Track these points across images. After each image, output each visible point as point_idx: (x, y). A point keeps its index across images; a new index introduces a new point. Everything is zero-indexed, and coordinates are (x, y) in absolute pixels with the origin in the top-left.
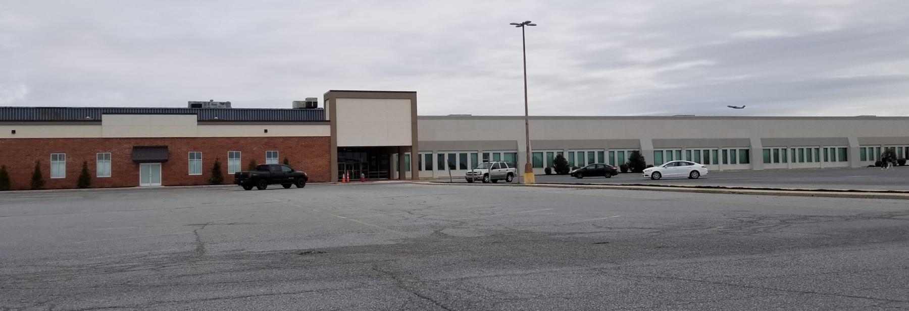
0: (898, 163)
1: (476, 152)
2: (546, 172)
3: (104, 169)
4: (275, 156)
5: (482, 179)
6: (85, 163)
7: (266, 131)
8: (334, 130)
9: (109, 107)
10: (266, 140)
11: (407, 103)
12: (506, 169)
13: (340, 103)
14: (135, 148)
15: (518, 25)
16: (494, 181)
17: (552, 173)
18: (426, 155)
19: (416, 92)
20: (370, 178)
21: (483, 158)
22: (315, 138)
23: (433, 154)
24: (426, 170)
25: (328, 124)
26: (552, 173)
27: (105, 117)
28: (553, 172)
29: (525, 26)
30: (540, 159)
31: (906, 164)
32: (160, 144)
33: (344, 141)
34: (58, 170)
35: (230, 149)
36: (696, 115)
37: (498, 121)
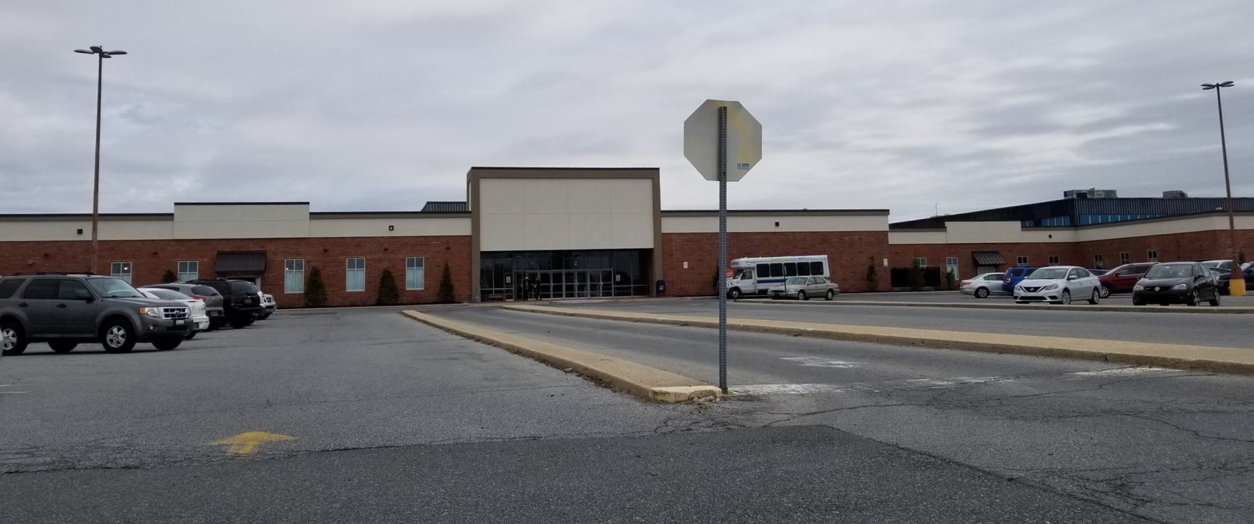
4: (193, 268)
7: (777, 224)
8: (476, 226)
9: (1137, 197)
11: (647, 184)
15: (1209, 87)
19: (658, 169)
20: (567, 297)
22: (48, 245)
25: (1226, 215)
33: (489, 243)
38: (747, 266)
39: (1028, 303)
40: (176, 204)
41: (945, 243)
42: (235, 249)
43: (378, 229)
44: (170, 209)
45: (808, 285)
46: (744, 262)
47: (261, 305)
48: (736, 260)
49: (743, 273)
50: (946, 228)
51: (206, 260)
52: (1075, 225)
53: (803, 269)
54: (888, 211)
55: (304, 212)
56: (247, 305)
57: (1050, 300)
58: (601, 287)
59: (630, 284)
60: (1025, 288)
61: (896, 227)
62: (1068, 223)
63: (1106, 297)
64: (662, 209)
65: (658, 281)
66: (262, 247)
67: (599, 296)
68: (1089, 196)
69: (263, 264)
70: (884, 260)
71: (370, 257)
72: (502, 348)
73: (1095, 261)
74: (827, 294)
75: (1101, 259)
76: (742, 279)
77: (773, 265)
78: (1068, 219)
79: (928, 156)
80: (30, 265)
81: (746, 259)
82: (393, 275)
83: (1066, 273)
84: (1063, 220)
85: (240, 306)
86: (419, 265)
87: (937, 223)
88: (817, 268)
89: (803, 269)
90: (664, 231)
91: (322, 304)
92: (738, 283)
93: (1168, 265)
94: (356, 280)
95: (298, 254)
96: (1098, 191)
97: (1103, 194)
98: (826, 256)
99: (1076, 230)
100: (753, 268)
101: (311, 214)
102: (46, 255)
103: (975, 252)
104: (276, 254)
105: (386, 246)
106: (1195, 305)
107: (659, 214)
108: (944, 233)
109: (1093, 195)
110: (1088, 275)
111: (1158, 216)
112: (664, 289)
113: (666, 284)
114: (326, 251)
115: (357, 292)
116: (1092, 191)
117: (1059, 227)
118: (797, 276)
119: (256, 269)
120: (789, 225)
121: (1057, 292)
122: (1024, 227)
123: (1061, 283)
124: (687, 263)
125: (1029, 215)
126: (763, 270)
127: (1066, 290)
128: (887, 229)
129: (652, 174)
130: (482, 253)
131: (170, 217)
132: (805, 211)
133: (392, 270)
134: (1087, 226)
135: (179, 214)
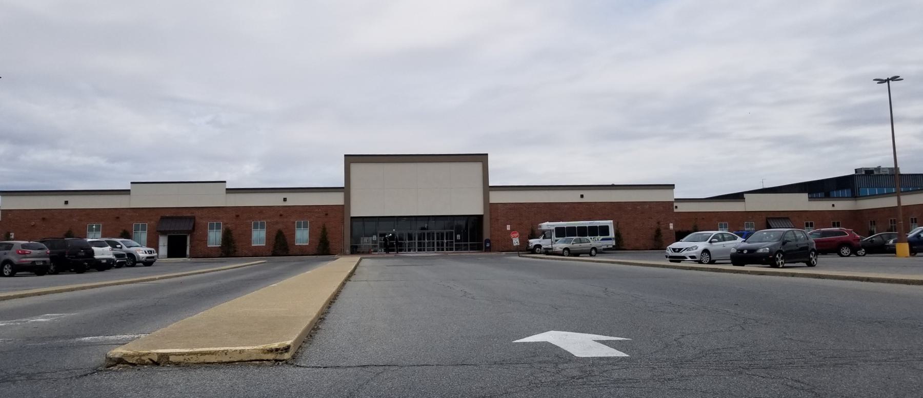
5: (589, 251)
8: (347, 198)
9: (906, 173)
11: (478, 166)
15: (881, 81)
16: (577, 254)
19: (487, 154)
22: (719, 213)
29: (890, 81)
30: (886, 235)
36: (615, 184)
38: (548, 228)
39: (679, 262)
40: (132, 183)
41: (744, 210)
42: (172, 215)
43: (275, 200)
44: (127, 186)
45: (573, 244)
46: (546, 225)
47: (95, 257)
48: (540, 224)
49: (545, 234)
50: (744, 199)
51: (152, 222)
52: (855, 196)
53: (593, 231)
54: (674, 185)
55: (221, 189)
56: (80, 257)
57: (690, 259)
58: (445, 244)
59: (470, 244)
60: (673, 249)
61: (678, 200)
62: (850, 195)
63: (864, 255)
64: (490, 185)
65: (487, 240)
66: (192, 213)
67: (406, 251)
68: (875, 173)
69: (192, 224)
70: (670, 224)
71: (269, 221)
72: (50, 293)
73: (870, 226)
74: (591, 251)
75: (874, 225)
76: (543, 238)
77: (590, 227)
78: (850, 191)
79: (797, 143)
80: (32, 226)
81: (547, 223)
82: (285, 234)
83: (710, 236)
84: (846, 192)
85: (72, 258)
86: (305, 227)
87: (738, 197)
88: (604, 231)
89: (593, 231)
90: (491, 201)
91: (233, 255)
92: (540, 242)
93: (765, 232)
94: (259, 237)
95: (218, 219)
96: (883, 169)
97: (888, 171)
98: (612, 221)
99: (856, 200)
100: (553, 231)
101: (227, 189)
102: (44, 219)
103: (769, 218)
104: (201, 218)
105: (281, 212)
106: (777, 267)
107: (488, 189)
108: (744, 203)
109: (879, 172)
110: (735, 239)
111: (911, 189)
112: (490, 245)
113: (491, 242)
114: (237, 216)
115: (260, 246)
116: (879, 169)
117: (843, 198)
118: (566, 237)
119: (186, 229)
120: (591, 197)
121: (696, 253)
122: (811, 199)
123: (702, 246)
124: (672, 224)
125: (815, 189)
126: (560, 232)
127: (706, 251)
128: (673, 200)
129: (482, 158)
130: (352, 218)
131: (128, 192)
132: (613, 186)
133: (284, 231)
134: (866, 197)
135: (135, 190)
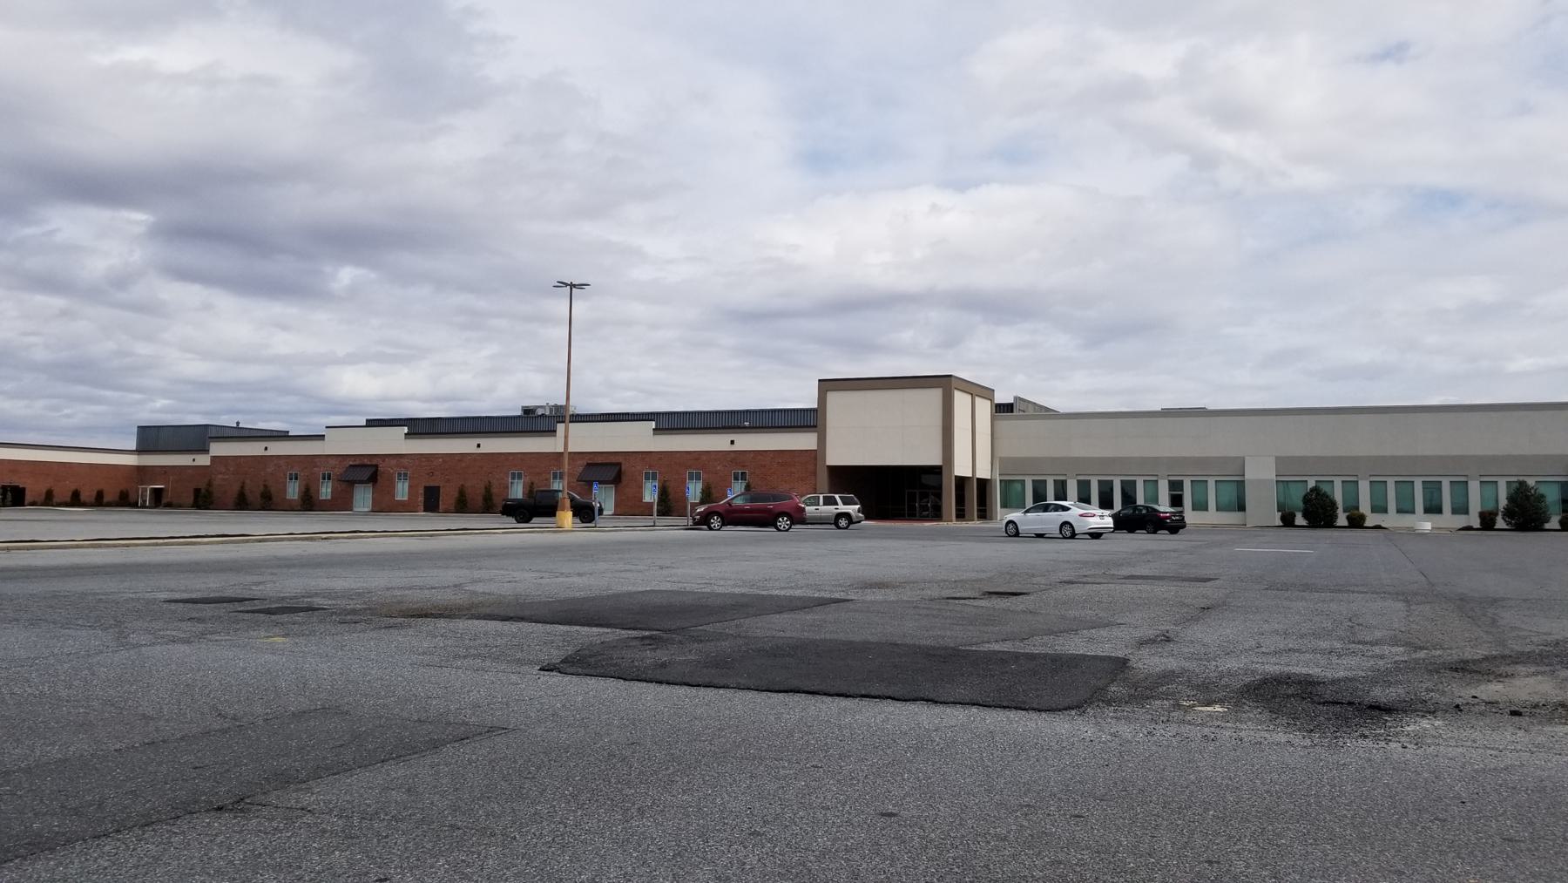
0: (1305, 516)
1: (1155, 478)
2: (1349, 522)
3: (326, 491)
6: (532, 483)
8: (822, 441)
9: (643, 411)
10: (733, 455)
12: (836, 507)
13: (833, 398)
14: (588, 464)
17: (1297, 523)
18: (1033, 481)
21: (1170, 490)
23: (1360, 482)
24: (1193, 509)
26: (1297, 523)
27: (365, 424)
28: (1300, 520)
31: (1496, 527)
32: (613, 460)
33: (838, 456)
34: (293, 491)
35: (690, 467)
37: (1305, 418)
